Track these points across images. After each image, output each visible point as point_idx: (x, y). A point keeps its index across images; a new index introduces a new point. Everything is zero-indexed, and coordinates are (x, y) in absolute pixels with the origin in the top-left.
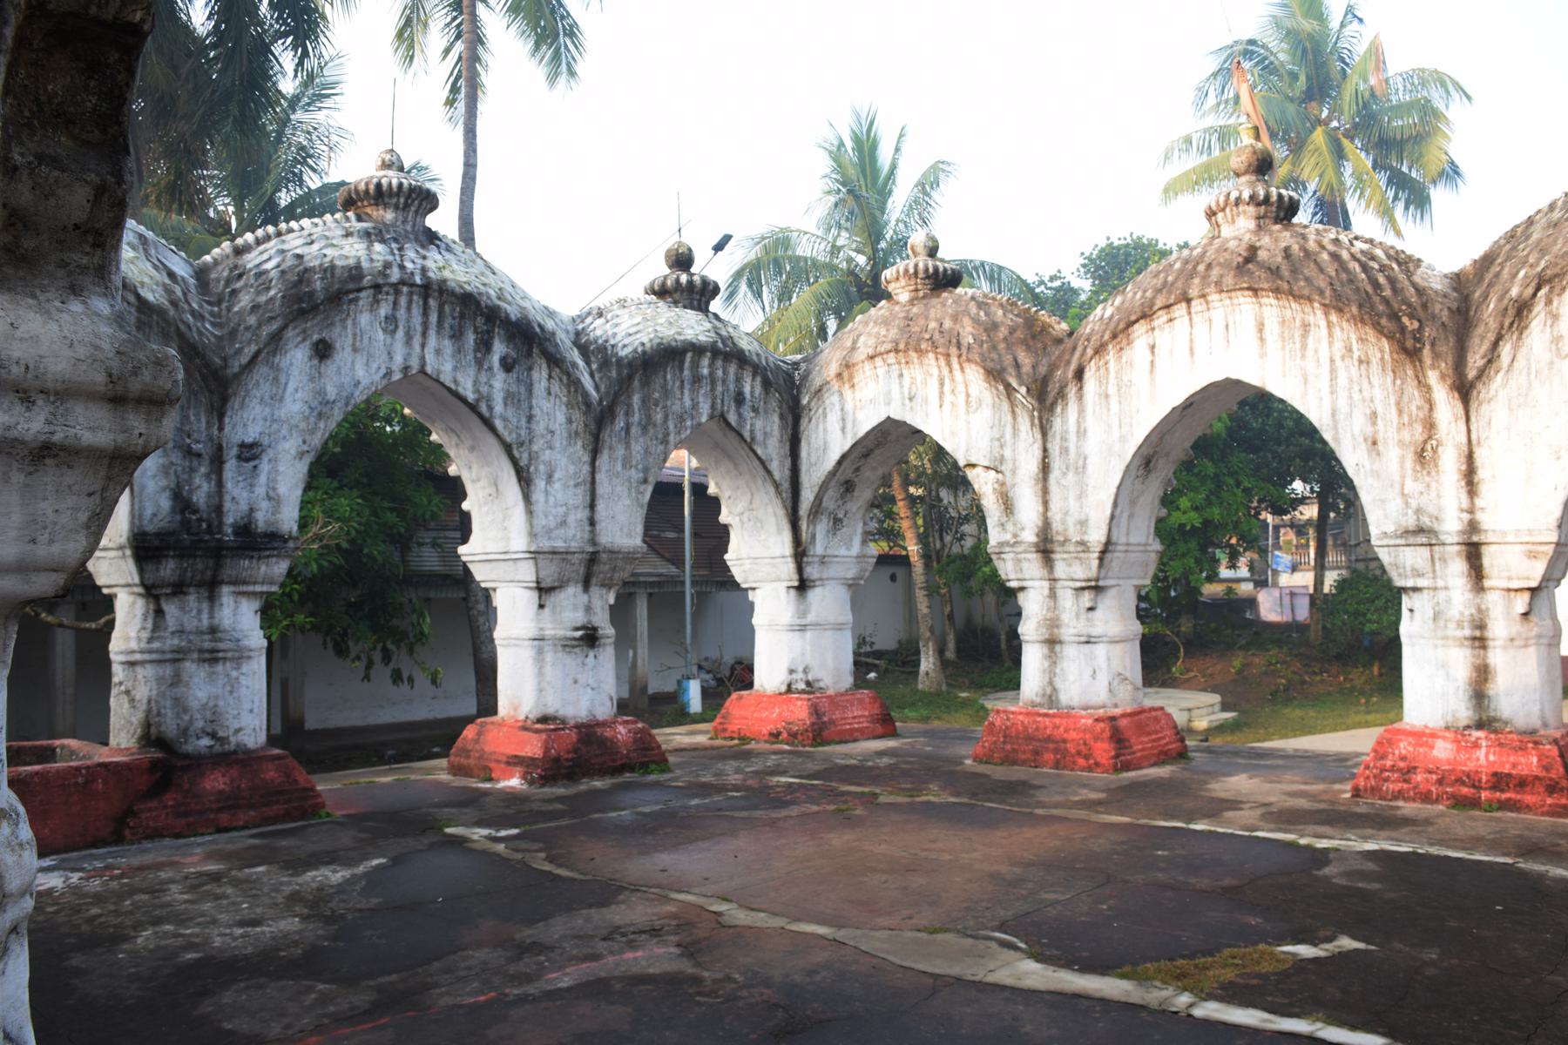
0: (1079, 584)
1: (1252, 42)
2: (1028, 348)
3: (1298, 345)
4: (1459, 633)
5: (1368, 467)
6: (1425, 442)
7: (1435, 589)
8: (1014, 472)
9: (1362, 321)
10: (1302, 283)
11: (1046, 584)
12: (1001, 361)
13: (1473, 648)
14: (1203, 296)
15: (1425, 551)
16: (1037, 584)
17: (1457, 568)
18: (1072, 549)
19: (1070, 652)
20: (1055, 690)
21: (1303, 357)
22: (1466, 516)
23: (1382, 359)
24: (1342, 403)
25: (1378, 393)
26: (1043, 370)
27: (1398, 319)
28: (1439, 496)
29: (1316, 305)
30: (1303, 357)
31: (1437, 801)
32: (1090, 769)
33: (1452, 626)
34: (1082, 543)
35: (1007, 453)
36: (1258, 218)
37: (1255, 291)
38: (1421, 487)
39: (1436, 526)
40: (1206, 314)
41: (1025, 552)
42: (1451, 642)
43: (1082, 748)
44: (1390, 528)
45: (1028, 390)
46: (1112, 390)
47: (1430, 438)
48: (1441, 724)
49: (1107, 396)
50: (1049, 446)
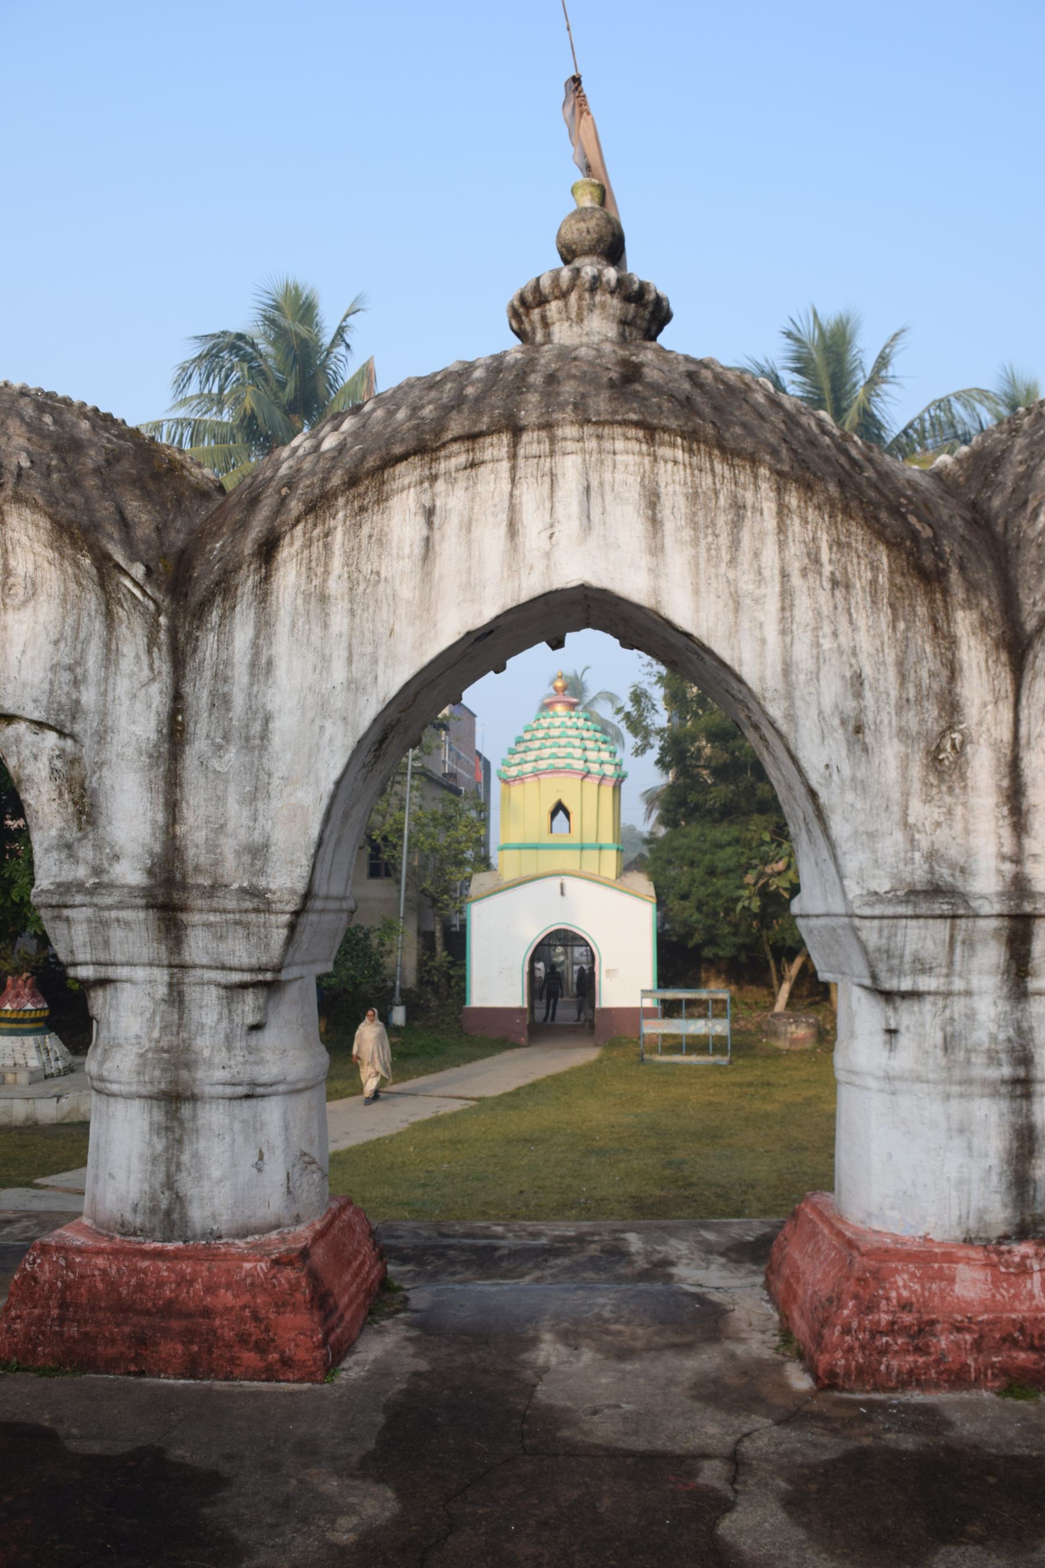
0: (236, 977)
1: (240, 337)
2: (146, 496)
3: (724, 540)
4: (994, 1073)
5: (847, 771)
6: (942, 735)
7: (948, 994)
8: (102, 736)
9: (847, 512)
10: (738, 430)
11: (162, 976)
12: (88, 507)
13: (1013, 1097)
14: (548, 426)
15: (940, 930)
16: (140, 973)
17: (990, 956)
18: (231, 904)
19: (213, 1117)
20: (179, 1199)
21: (733, 562)
22: (1008, 867)
23: (874, 582)
24: (802, 652)
25: (865, 641)
26: (178, 538)
27: (903, 517)
28: (967, 831)
29: (763, 471)
30: (733, 562)
31: (977, 1383)
32: (270, 1374)
33: (978, 1059)
34: (253, 892)
35: (89, 697)
36: (623, 322)
37: (650, 431)
38: (936, 813)
39: (960, 883)
40: (546, 463)
41: (120, 906)
42: (976, 1089)
43: (250, 1327)
44: (883, 885)
45: (149, 572)
46: (335, 586)
47: (951, 728)
48: (958, 1234)
49: (323, 599)
50: (187, 688)
